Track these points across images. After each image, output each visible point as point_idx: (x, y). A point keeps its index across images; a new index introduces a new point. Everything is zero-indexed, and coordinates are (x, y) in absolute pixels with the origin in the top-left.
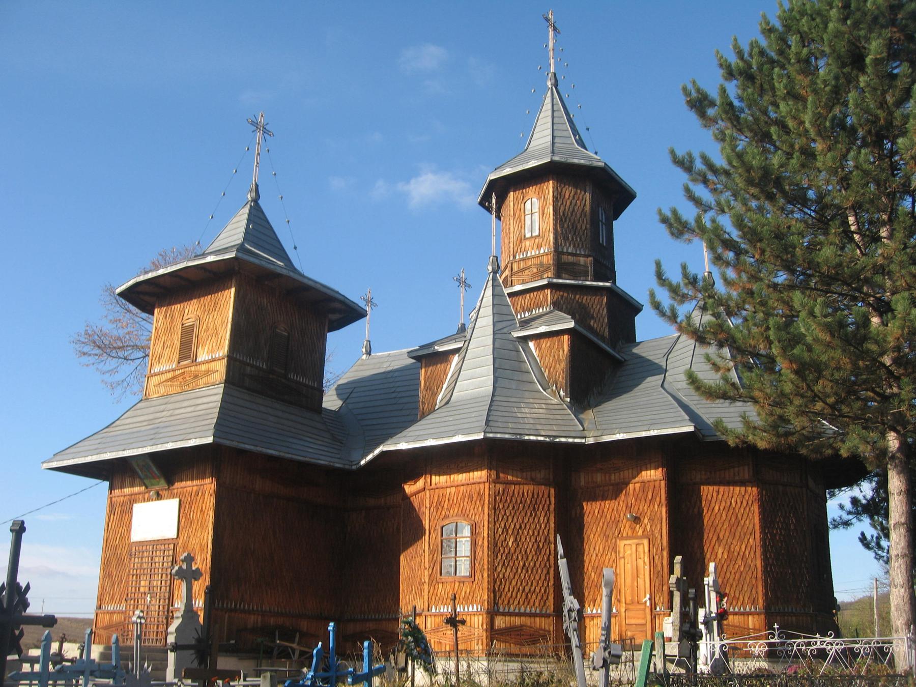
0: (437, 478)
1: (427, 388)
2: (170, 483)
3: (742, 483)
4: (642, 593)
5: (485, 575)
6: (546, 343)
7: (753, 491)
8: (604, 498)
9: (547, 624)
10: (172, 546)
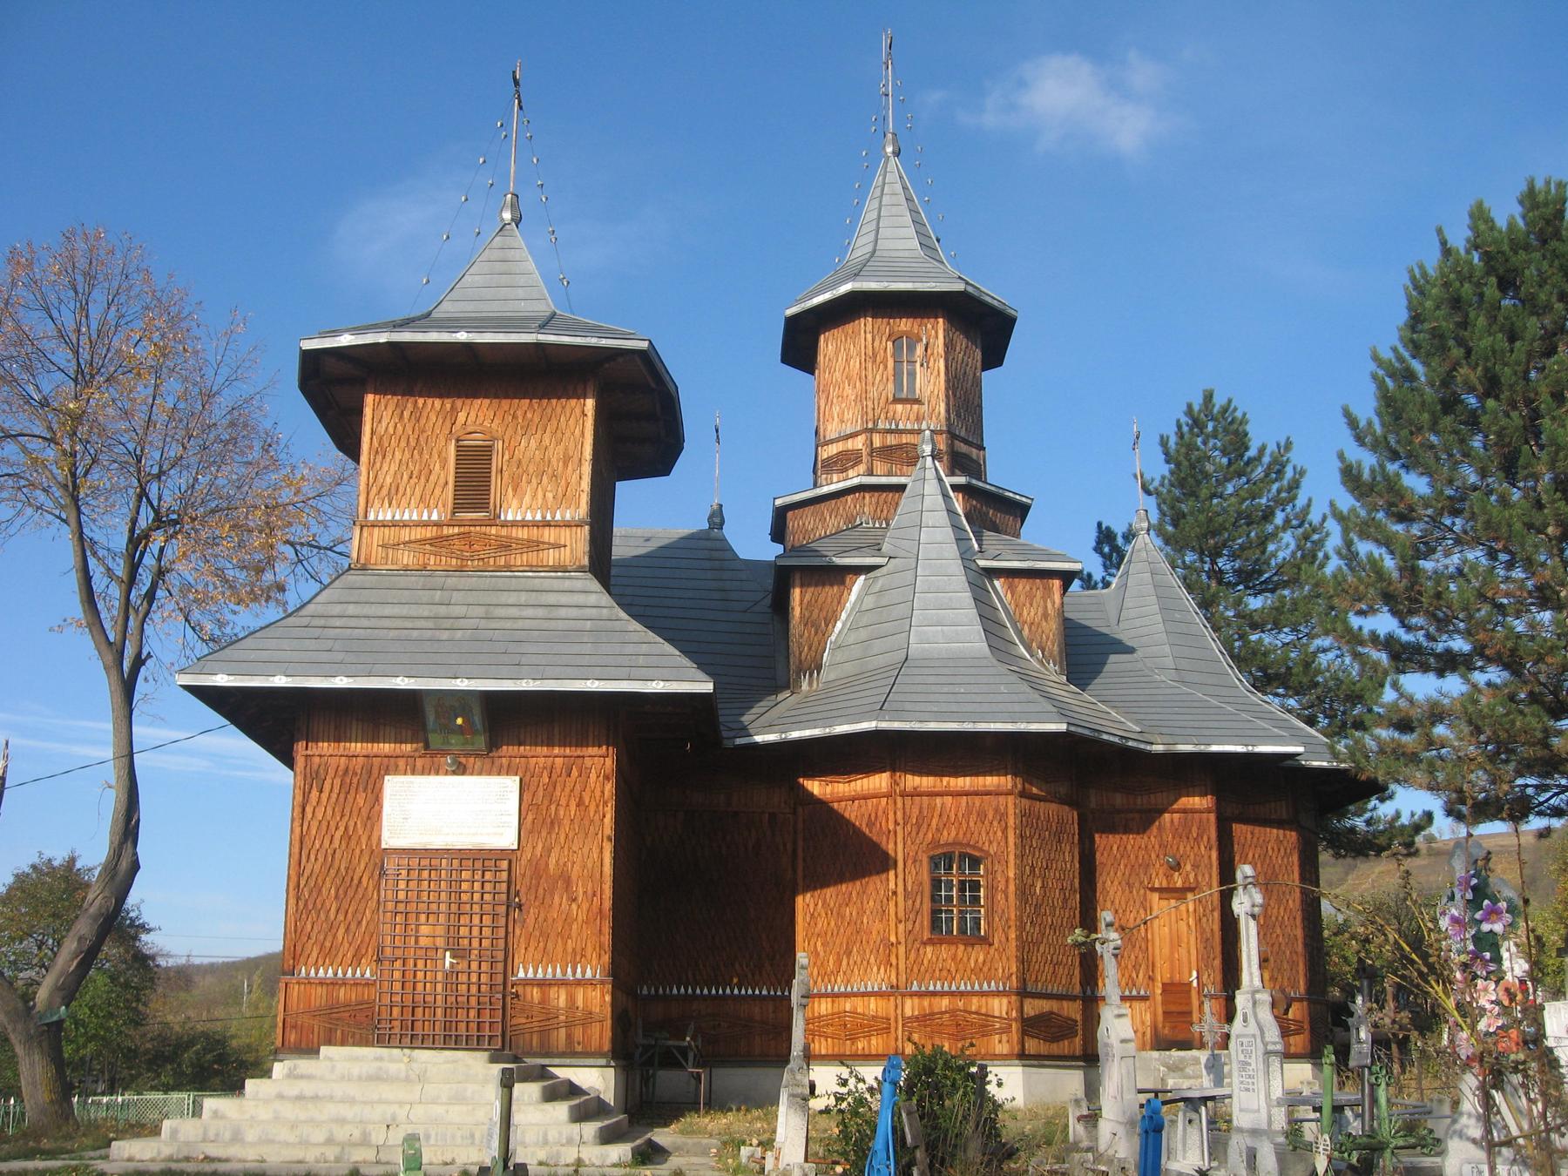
0: (917, 779)
1: (806, 621)
2: (493, 744)
3: (1279, 824)
4: (1186, 970)
5: (1013, 936)
6: (1022, 585)
7: (1292, 836)
8: (1127, 830)
9: (1073, 1010)
10: (505, 864)
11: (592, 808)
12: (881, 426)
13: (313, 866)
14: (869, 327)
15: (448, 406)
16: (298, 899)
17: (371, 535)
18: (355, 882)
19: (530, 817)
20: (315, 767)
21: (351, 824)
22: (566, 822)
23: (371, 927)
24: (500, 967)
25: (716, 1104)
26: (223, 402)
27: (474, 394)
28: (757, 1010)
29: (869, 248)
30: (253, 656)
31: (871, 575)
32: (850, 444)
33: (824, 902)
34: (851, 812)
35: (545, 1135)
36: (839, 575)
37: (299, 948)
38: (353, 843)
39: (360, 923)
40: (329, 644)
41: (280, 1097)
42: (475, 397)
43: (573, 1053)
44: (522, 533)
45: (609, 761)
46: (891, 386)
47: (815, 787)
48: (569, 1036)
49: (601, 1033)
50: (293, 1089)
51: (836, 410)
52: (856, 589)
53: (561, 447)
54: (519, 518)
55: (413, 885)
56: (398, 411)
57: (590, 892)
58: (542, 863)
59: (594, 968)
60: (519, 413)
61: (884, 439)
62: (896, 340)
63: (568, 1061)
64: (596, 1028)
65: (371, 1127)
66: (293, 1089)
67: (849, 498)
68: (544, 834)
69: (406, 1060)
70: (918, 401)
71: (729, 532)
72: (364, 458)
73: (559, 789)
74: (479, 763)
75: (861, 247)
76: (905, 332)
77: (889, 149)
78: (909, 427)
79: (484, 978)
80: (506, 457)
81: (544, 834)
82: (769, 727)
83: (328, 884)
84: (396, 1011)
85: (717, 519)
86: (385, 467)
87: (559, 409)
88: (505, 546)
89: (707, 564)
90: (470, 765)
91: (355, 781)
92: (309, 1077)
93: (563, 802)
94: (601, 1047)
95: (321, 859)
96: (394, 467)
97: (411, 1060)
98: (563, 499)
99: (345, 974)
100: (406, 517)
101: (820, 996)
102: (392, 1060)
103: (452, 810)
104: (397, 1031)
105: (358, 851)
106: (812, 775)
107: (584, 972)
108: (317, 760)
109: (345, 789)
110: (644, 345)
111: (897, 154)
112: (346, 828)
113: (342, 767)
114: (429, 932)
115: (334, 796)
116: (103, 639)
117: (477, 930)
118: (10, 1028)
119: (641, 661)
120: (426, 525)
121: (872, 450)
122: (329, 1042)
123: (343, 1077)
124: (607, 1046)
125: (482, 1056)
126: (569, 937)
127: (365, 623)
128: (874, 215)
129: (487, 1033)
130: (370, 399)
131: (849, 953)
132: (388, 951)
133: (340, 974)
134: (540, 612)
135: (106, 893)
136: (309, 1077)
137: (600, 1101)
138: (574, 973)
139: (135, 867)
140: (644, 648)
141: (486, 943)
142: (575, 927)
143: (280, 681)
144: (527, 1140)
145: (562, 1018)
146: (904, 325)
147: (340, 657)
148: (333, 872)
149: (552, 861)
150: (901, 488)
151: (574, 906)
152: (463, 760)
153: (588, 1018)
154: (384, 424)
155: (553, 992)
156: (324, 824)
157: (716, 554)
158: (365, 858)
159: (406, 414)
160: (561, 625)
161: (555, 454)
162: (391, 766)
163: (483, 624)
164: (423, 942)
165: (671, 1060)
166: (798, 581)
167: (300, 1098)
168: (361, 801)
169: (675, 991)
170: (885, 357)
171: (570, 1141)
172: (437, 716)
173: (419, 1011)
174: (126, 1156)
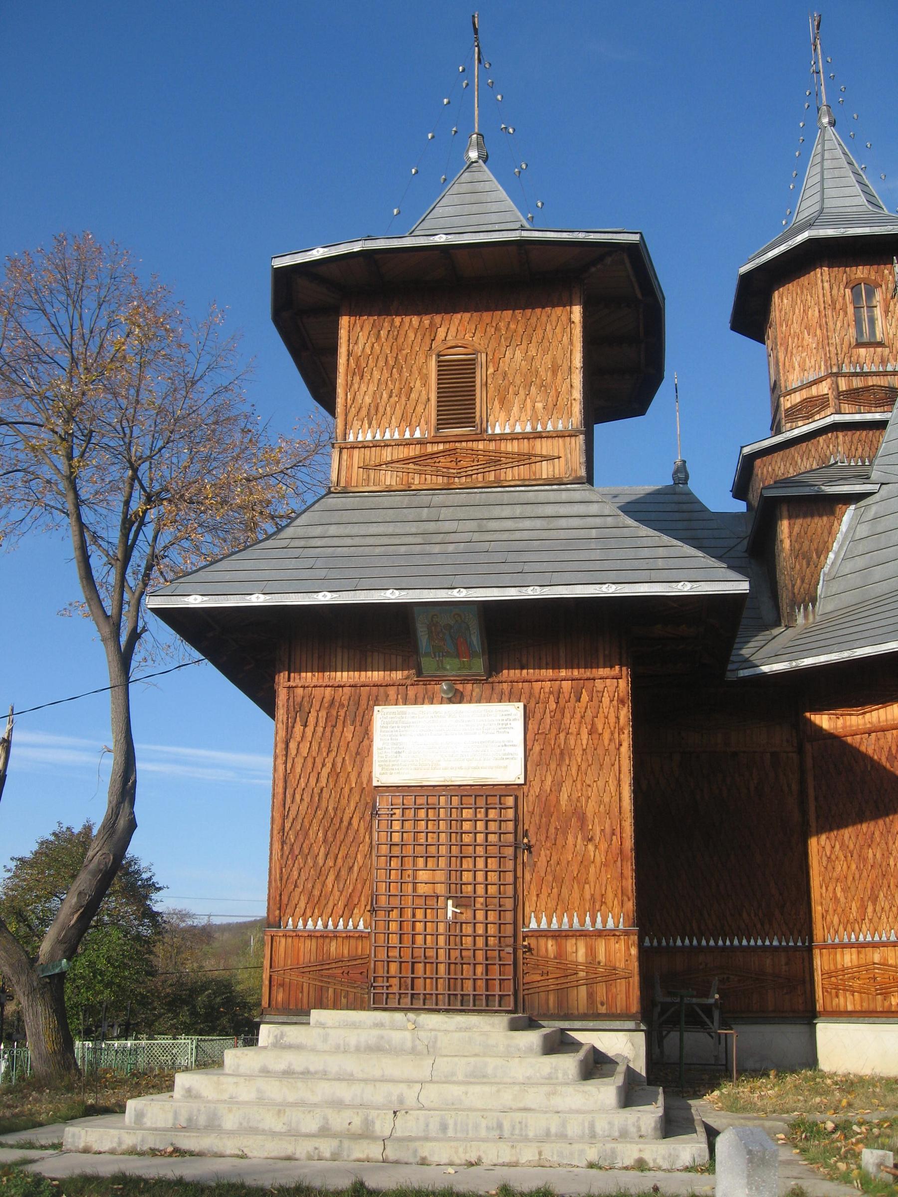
1: (797, 554)
2: (493, 669)
10: (510, 801)
11: (606, 736)
12: (845, 370)
13: (300, 807)
14: (826, 278)
15: (427, 322)
16: (283, 843)
17: (351, 457)
18: (345, 823)
19: (537, 748)
20: (299, 699)
21: (339, 760)
22: (578, 752)
23: (364, 874)
24: (509, 917)
25: (756, 1070)
26: (205, 389)
27: (452, 309)
28: (768, 961)
29: (817, 207)
30: (228, 576)
31: (862, 503)
32: (814, 391)
33: (842, 844)
34: (868, 746)
35: (592, 1126)
36: (829, 504)
38: (342, 780)
39: (351, 868)
40: (310, 563)
41: (265, 1072)
42: (455, 312)
43: (600, 1016)
44: (511, 447)
46: (852, 331)
47: (824, 721)
48: (591, 996)
49: (627, 993)
50: (280, 1062)
51: (796, 361)
52: (846, 518)
53: (548, 358)
54: (507, 431)
55: (408, 826)
56: (375, 331)
57: (608, 831)
59: (616, 916)
60: (502, 325)
61: (849, 383)
62: (855, 287)
63: (591, 1024)
64: (621, 985)
65: (373, 1113)
66: (280, 1062)
67: (821, 439)
68: (553, 766)
69: (410, 1026)
70: (880, 344)
71: (693, 486)
72: (339, 409)
73: (567, 715)
74: (477, 689)
75: (807, 208)
76: (863, 279)
77: (825, 120)
78: (874, 369)
79: (492, 930)
80: (491, 370)
81: (553, 766)
82: (776, 657)
83: (315, 827)
84: (394, 967)
85: (681, 474)
86: (363, 388)
87: (544, 318)
88: (495, 461)
89: (677, 516)
90: (467, 693)
91: (342, 713)
92: (297, 1047)
93: (573, 729)
94: (628, 1007)
95: (307, 798)
96: (372, 388)
97: (416, 1027)
98: (553, 408)
99: (336, 926)
100: (387, 436)
101: (843, 946)
102: (394, 1027)
103: (450, 741)
104: (395, 989)
105: (346, 790)
106: (820, 709)
107: (604, 922)
108: (300, 691)
109: (332, 722)
110: (636, 238)
111: (833, 124)
113: (328, 698)
114: (429, 878)
115: (320, 730)
116: (101, 612)
117: (480, 875)
118: (14, 980)
119: (660, 563)
120: (408, 443)
121: (839, 394)
123: (338, 1047)
124: (635, 1007)
125: (502, 1020)
126: (587, 882)
127: (349, 541)
128: (818, 178)
129: (497, 992)
130: (344, 321)
131: (874, 899)
132: (383, 901)
134: (538, 523)
135: (105, 850)
136: (297, 1047)
138: (594, 922)
139: (132, 825)
140: (661, 552)
141: (492, 890)
142: (592, 870)
143: (257, 600)
144: (570, 1133)
145: (582, 974)
146: (861, 272)
147: (323, 573)
148: (320, 813)
149: (564, 797)
150: (882, 425)
151: (591, 847)
152: (460, 687)
153: (611, 975)
154: (361, 345)
155: (570, 944)
157: (685, 507)
158: (355, 798)
159: (383, 333)
160: (562, 534)
161: (543, 364)
162: (380, 695)
163: (476, 537)
164: (422, 889)
165: (696, 1019)
166: (785, 513)
167: (288, 1074)
168: (348, 735)
169: (679, 943)
170: (845, 304)
171: (624, 1135)
172: (431, 638)
173: (420, 967)
174: (81, 1145)
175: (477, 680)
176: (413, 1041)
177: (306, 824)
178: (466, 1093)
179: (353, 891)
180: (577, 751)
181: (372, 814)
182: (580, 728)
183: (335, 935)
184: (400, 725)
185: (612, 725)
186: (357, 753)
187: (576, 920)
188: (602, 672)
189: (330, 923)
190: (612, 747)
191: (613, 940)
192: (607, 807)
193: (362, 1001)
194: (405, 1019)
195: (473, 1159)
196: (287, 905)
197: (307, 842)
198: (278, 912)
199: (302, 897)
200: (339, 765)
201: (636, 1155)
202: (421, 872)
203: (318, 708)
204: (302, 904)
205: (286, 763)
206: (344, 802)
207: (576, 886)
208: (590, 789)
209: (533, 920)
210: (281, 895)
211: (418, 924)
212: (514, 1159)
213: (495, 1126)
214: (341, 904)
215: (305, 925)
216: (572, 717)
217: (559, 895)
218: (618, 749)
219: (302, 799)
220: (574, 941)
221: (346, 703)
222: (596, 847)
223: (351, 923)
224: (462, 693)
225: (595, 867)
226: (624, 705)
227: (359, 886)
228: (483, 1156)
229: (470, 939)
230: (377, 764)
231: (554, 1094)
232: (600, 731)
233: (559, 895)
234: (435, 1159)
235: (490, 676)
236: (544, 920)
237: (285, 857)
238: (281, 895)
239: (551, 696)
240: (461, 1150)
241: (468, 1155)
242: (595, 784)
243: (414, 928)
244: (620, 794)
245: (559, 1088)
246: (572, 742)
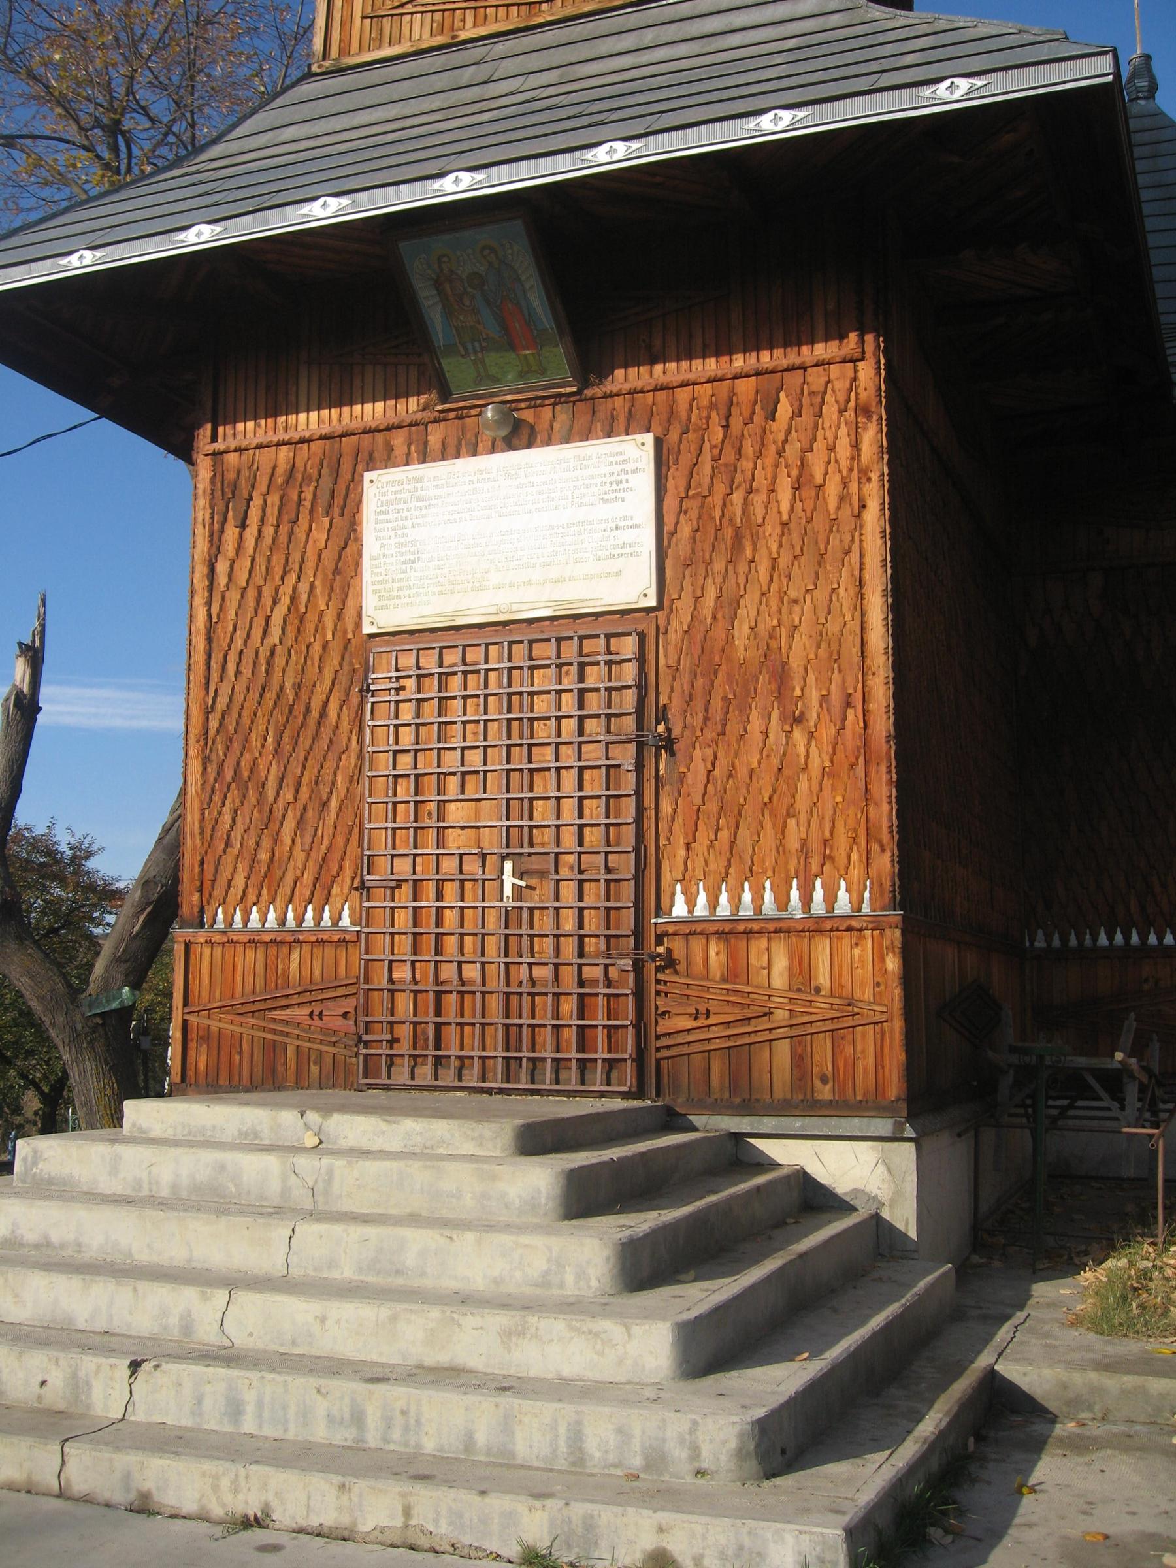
2: (591, 365)
10: (628, 647)
11: (832, 489)
16: (206, 760)
18: (315, 714)
20: (231, 476)
21: (304, 588)
22: (771, 530)
24: (627, 892)
37: (209, 868)
39: (325, 804)
45: (866, 370)
48: (799, 1061)
49: (879, 1053)
57: (836, 698)
58: (719, 633)
63: (796, 1124)
68: (719, 566)
73: (749, 449)
74: (563, 415)
79: (592, 922)
81: (719, 566)
83: (261, 720)
84: (404, 1004)
90: (542, 426)
91: (308, 494)
93: (761, 480)
95: (246, 670)
99: (300, 920)
103: (512, 529)
104: (405, 1048)
105: (317, 648)
108: (232, 458)
109: (289, 514)
112: (293, 599)
113: (282, 467)
115: (269, 531)
122: (51, 1124)
124: (894, 1087)
126: (791, 813)
133: (291, 922)
137: (878, 1229)
138: (807, 900)
141: (593, 837)
142: (803, 786)
145: (781, 1015)
148: (270, 696)
149: (742, 631)
151: (799, 736)
152: (527, 415)
156: (251, 593)
158: (333, 662)
162: (376, 449)
168: (319, 536)
169: (1103, 940)
175: (561, 395)
176: (284, 1178)
177: (246, 721)
178: (323, 1320)
179: (329, 848)
180: (768, 529)
181: (361, 691)
182: (775, 477)
183: (296, 941)
184: (412, 505)
185: (844, 464)
186: (336, 571)
187: (768, 896)
188: (821, 350)
189: (290, 915)
190: (846, 513)
191: (846, 939)
192: (835, 647)
193: (348, 1071)
194: (300, 1122)
195: (253, 1510)
196: (213, 882)
197: (247, 756)
198: (196, 896)
199: (239, 865)
200: (303, 598)
201: (648, 1542)
202: (453, 806)
203: (264, 489)
204: (240, 881)
205: (209, 604)
206: (312, 670)
207: (768, 823)
208: (797, 608)
209: (680, 899)
210: (202, 863)
211: (447, 912)
212: (345, 1520)
213: (347, 1416)
214: (308, 878)
215: (246, 921)
216: (759, 455)
217: (733, 843)
218: (859, 516)
219: (238, 672)
220: (763, 943)
221: (313, 472)
222: (811, 735)
223: (327, 914)
224: (532, 427)
225: (810, 780)
226: (869, 418)
227: (340, 840)
228: (275, 1504)
229: (549, 943)
230: (371, 588)
231: (521, 1334)
232: (819, 480)
233: (733, 843)
234: (168, 1498)
235: (585, 384)
236: (702, 899)
237: (209, 789)
238: (202, 863)
239: (714, 414)
240: (225, 1483)
241: (241, 1497)
242: (808, 598)
243: (439, 923)
244: (863, 615)
245: (532, 1320)
246: (759, 511)
